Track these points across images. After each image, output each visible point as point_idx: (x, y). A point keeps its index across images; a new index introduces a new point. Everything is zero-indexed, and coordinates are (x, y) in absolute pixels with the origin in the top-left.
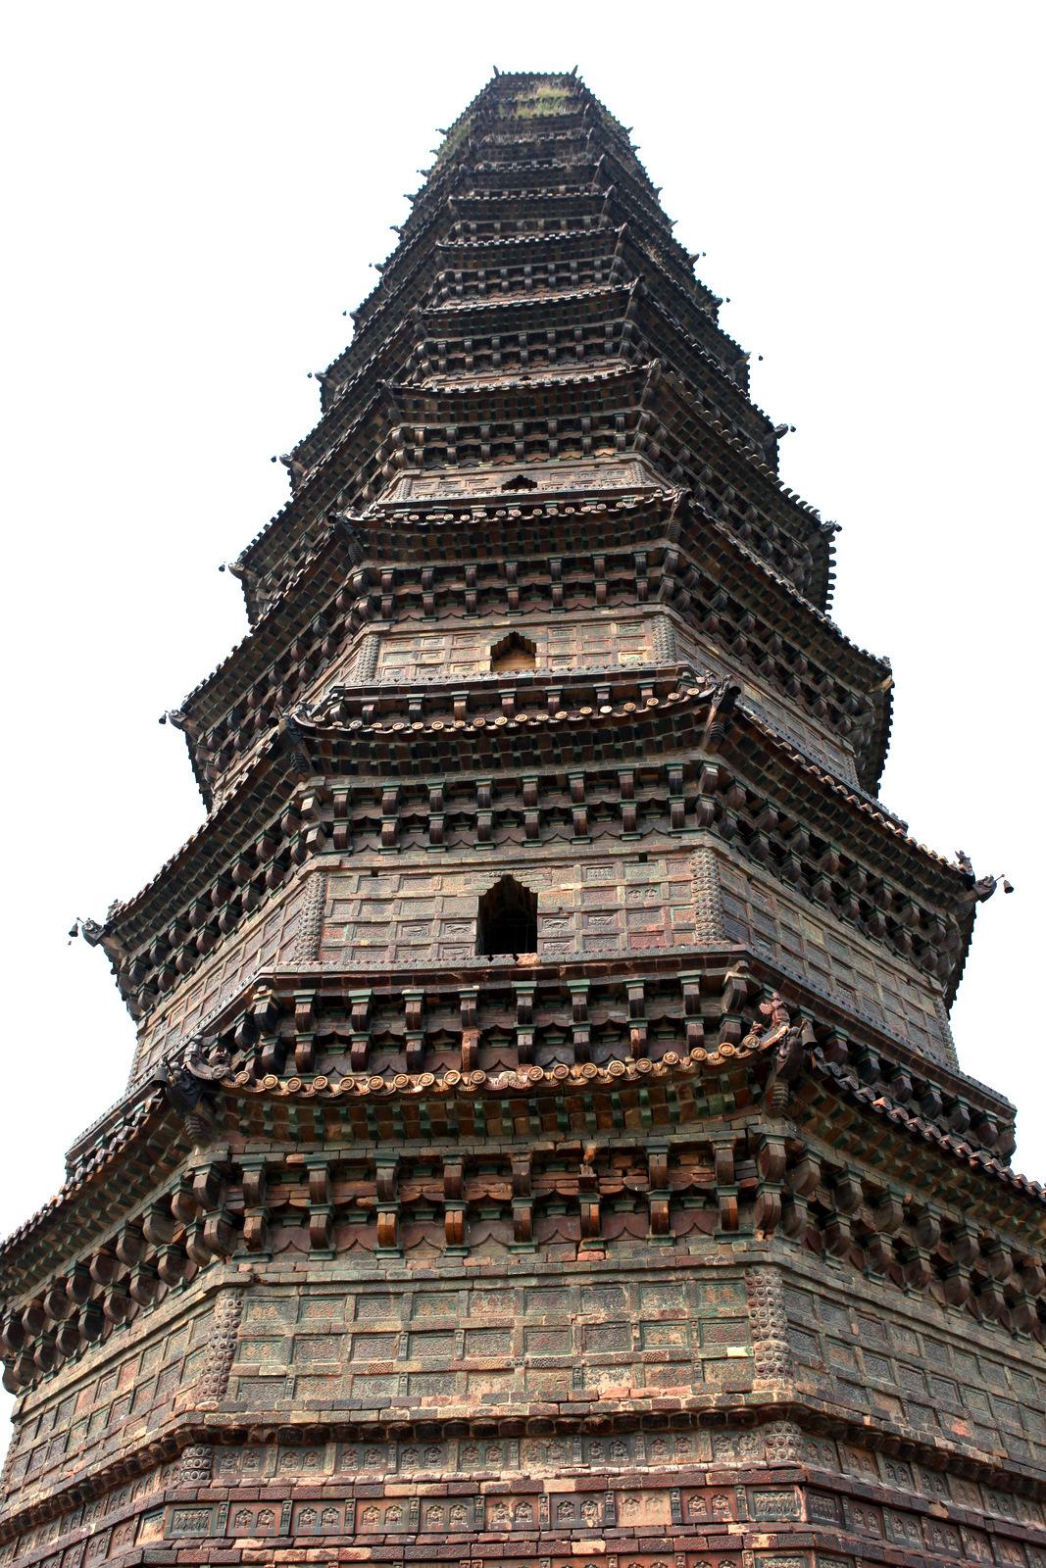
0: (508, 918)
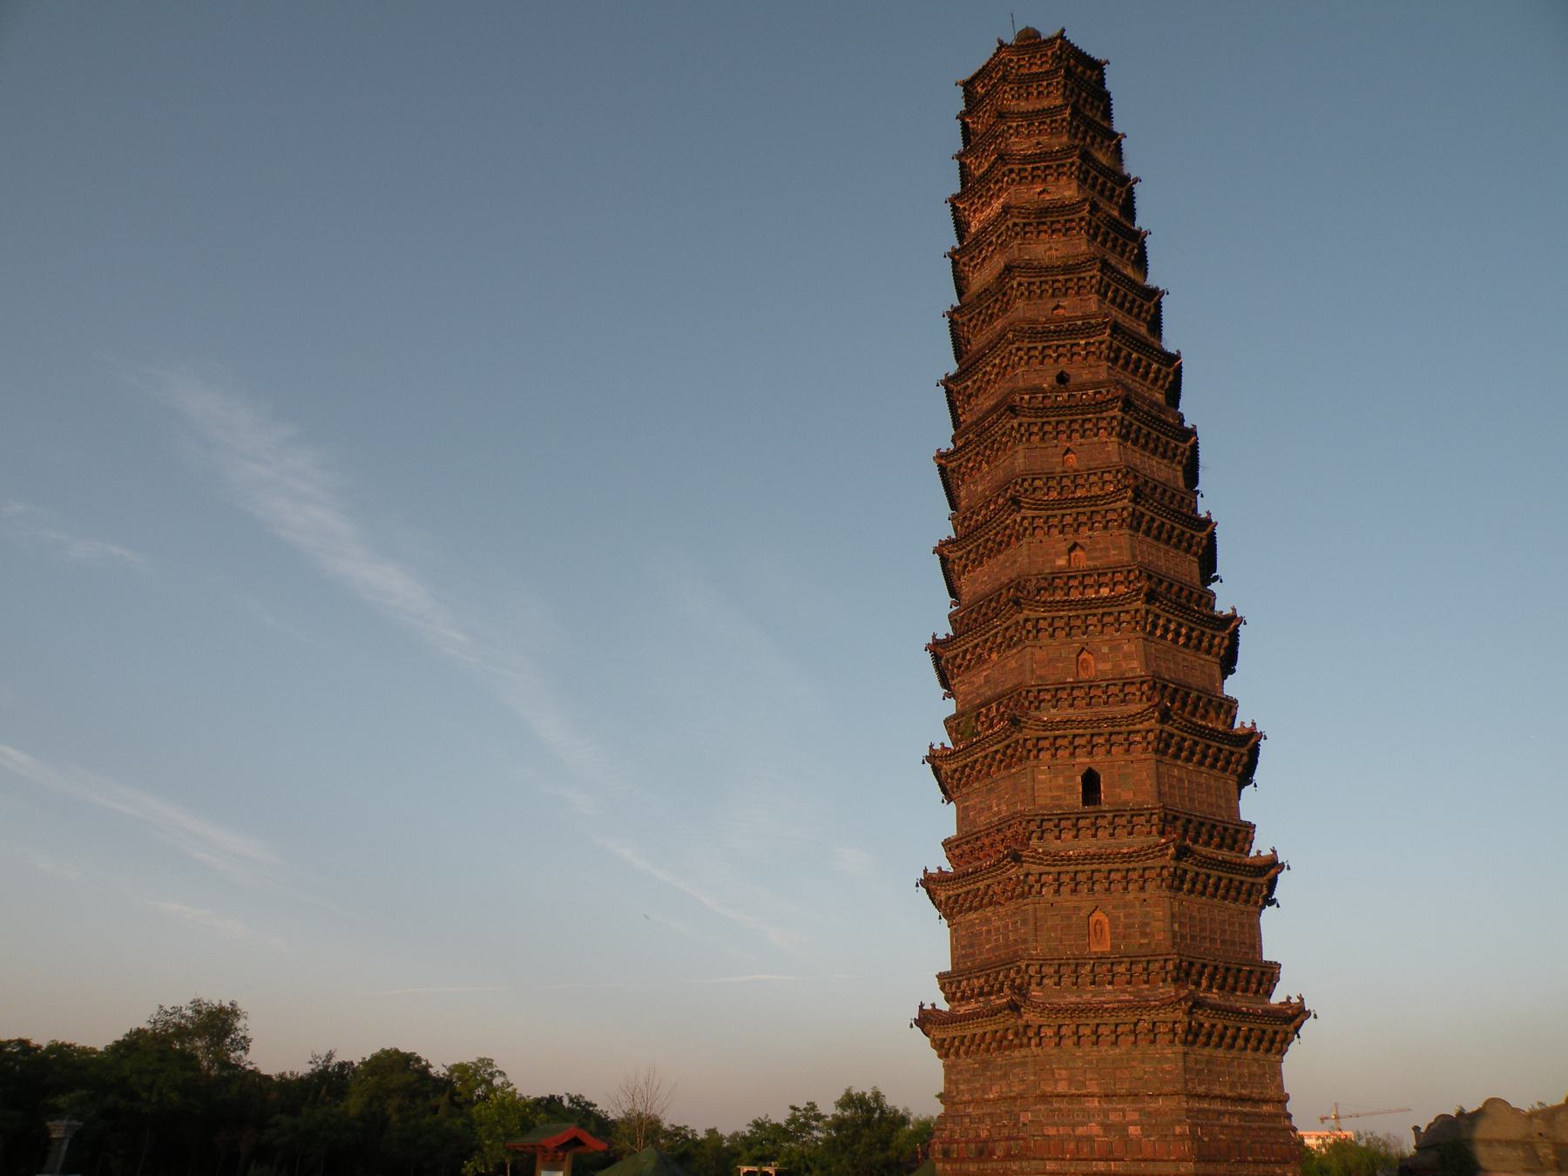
0: (1091, 782)
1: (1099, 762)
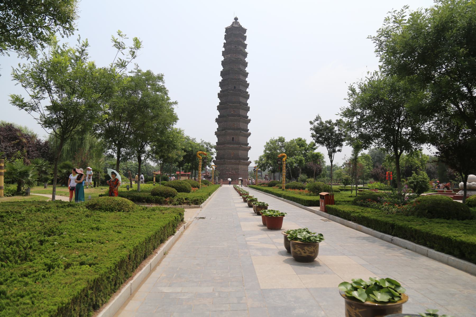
0: (235, 87)
1: (234, 136)
